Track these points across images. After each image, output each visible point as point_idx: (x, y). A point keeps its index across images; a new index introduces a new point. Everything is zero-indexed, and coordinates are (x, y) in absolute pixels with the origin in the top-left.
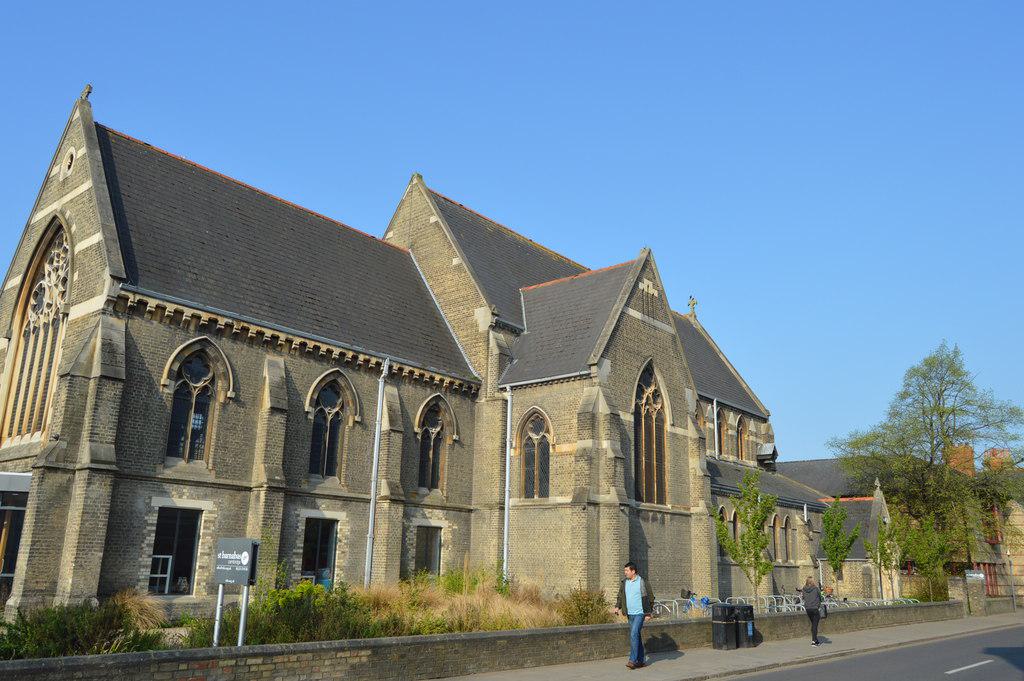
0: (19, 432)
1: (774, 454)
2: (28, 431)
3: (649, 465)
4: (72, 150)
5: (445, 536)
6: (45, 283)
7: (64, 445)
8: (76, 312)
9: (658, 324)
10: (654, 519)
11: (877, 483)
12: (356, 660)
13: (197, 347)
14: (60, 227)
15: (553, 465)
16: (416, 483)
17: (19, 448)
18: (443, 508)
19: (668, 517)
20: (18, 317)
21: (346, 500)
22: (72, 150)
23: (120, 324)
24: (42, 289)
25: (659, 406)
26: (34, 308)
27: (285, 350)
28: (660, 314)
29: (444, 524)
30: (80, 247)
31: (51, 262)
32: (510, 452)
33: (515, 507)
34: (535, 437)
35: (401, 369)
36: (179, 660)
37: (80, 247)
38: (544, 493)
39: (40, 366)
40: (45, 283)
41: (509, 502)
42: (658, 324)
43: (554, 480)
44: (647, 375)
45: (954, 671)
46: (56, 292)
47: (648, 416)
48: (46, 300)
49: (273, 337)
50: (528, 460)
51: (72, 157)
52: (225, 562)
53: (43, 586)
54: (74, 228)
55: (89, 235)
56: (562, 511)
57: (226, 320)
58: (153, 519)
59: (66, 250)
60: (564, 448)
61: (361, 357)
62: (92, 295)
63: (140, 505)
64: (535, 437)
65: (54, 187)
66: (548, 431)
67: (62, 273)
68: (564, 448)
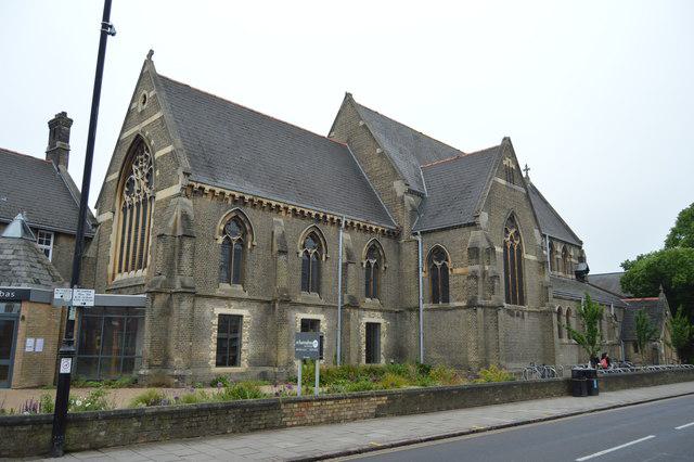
0: (126, 270)
1: (588, 270)
2: (133, 269)
3: (514, 279)
4: (145, 92)
5: (383, 328)
6: (134, 177)
7: (164, 277)
8: (161, 195)
9: (516, 187)
10: (518, 315)
11: (661, 288)
12: (380, 402)
13: (234, 214)
14: (142, 141)
15: (452, 282)
16: (364, 294)
17: (129, 280)
18: (380, 311)
19: (526, 314)
20: (118, 198)
21: (323, 307)
22: (145, 92)
23: (190, 202)
24: (132, 181)
25: (518, 242)
26: (128, 193)
27: (283, 214)
28: (517, 180)
29: (382, 321)
30: (158, 154)
31: (137, 164)
32: (421, 274)
33: (426, 310)
34: (437, 264)
35: (352, 223)
36: (295, 402)
37: (158, 154)
38: (446, 300)
39: (137, 228)
40: (134, 177)
41: (422, 306)
42: (516, 187)
43: (453, 292)
44: (512, 219)
45: (596, 455)
46: (143, 183)
47: (512, 248)
48: (136, 188)
49: (200, 188)
50: (434, 279)
51: (145, 96)
52: (302, 346)
53: (159, 363)
54: (153, 142)
55: (165, 146)
56: (459, 312)
57: (220, 190)
58: (216, 321)
59: (146, 156)
60: (459, 270)
61: (328, 217)
62: (171, 185)
63: (208, 312)
64: (437, 264)
65: (134, 116)
66: (447, 260)
67: (146, 171)
68: (459, 270)
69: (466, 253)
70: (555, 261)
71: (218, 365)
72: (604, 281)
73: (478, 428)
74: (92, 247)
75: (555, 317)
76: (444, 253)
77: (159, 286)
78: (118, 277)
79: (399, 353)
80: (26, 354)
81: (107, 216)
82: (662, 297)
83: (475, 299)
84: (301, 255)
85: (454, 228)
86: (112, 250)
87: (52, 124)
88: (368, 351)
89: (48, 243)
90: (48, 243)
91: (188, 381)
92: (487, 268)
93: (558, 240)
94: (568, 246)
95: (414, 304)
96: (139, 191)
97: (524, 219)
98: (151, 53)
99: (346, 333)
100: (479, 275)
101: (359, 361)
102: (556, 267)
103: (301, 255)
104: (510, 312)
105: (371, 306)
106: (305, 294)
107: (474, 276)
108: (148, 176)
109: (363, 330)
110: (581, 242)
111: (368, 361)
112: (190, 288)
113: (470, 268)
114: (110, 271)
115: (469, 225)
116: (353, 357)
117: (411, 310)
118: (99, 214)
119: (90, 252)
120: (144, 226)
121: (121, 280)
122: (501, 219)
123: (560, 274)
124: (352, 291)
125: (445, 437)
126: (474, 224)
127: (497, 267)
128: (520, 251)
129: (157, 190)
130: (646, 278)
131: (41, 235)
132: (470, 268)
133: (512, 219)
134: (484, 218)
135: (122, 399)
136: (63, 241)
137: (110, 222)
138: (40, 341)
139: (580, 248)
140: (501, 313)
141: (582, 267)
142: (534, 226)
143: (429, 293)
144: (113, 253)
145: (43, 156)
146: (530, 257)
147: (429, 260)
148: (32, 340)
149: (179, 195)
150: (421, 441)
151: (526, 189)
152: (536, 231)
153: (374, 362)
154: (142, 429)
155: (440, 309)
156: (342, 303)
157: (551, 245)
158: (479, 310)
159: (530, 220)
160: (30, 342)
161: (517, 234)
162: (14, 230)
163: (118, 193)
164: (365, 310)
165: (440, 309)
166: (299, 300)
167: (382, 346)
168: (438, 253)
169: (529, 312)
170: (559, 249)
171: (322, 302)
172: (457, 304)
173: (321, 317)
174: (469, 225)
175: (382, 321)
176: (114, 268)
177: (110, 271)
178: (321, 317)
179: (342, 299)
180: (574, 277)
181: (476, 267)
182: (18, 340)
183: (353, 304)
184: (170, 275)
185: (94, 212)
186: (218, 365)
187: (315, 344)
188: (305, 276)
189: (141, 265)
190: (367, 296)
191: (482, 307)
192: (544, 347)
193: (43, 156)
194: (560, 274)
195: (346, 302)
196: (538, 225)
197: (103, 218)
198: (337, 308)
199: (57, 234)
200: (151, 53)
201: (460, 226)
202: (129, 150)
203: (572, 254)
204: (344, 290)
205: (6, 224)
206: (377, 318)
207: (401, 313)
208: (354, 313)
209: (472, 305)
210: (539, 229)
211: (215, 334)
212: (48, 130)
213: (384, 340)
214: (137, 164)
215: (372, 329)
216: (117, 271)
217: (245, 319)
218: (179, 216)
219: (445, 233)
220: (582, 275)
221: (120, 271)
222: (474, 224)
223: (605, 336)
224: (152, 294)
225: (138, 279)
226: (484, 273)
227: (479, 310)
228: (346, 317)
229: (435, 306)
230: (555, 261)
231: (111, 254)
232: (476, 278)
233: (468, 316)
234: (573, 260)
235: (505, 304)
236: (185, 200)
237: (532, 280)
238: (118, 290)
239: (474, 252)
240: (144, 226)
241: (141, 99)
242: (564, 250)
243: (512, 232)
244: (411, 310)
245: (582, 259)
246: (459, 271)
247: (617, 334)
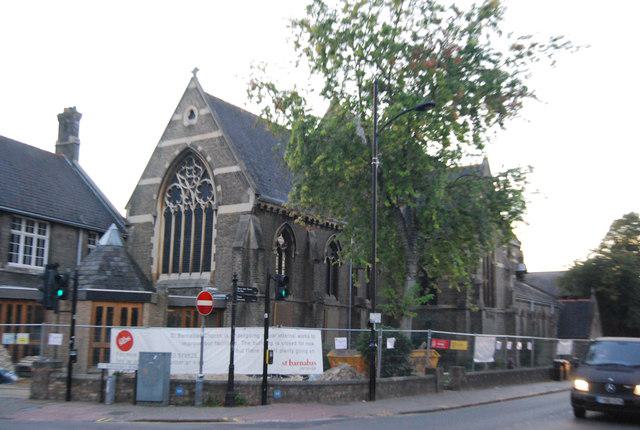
54: (209, 159)
62: (239, 201)
71: (381, 377)
72: (543, 282)
82: (593, 299)
87: (61, 118)
98: (195, 71)
110: (520, 243)
114: (154, 271)
118: (132, 213)
129: (219, 204)
130: (586, 278)
144: (157, 254)
145: (53, 150)
149: (248, 213)
156: (353, 304)
172: (445, 306)
176: (158, 268)
193: (53, 150)
199: (53, 224)
200: (195, 71)
202: (175, 160)
216: (161, 271)
221: (165, 271)
241: (187, 114)
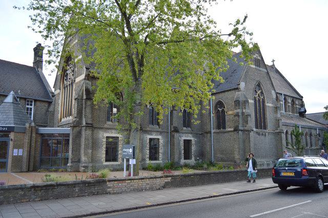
1: (305, 111)
5: (193, 142)
6: (68, 72)
10: (262, 135)
15: (227, 118)
16: (182, 125)
18: (191, 133)
20: (62, 83)
24: (67, 74)
28: (261, 65)
29: (192, 139)
30: (76, 60)
32: (212, 115)
38: (224, 128)
40: (68, 72)
42: (261, 69)
43: (227, 124)
47: (259, 100)
48: (69, 77)
56: (230, 133)
63: (100, 136)
66: (224, 107)
67: (72, 69)
68: (230, 112)
69: (233, 104)
70: (287, 107)
72: (315, 117)
73: (215, 194)
74: (52, 107)
75: (284, 136)
76: (223, 104)
77: (75, 124)
78: (63, 120)
79: (201, 154)
80: (13, 157)
81: (58, 91)
83: (238, 126)
84: (148, 107)
85: (227, 91)
86: (60, 107)
87: (35, 49)
88: (185, 153)
89: (31, 105)
90: (31, 105)
91: (90, 168)
92: (244, 111)
93: (289, 96)
94: (295, 102)
95: (209, 130)
96: (70, 79)
97: (266, 86)
99: (172, 144)
100: (240, 114)
101: (180, 159)
102: (288, 110)
103: (182, 111)
104: (258, 133)
105: (187, 131)
106: (151, 126)
107: (237, 115)
108: (73, 71)
109: (182, 143)
110: (302, 97)
111: (151, 158)
112: (90, 124)
113: (235, 111)
115: (235, 89)
116: (176, 156)
117: (207, 133)
119: (51, 109)
120: (72, 95)
121: (63, 124)
122: (252, 85)
123: (290, 113)
124: (175, 124)
125: (193, 200)
126: (237, 89)
127: (250, 110)
128: (264, 102)
131: (28, 101)
132: (235, 111)
133: (259, 85)
134: (242, 85)
135: (68, 177)
136: (38, 104)
137: (59, 94)
138: (21, 150)
139: (302, 100)
140: (252, 133)
141: (302, 110)
142: (272, 89)
143: (215, 124)
146: (269, 105)
147: (216, 107)
148: (17, 150)
150: (177, 202)
151: (267, 69)
152: (273, 92)
153: (189, 159)
154: (24, 195)
155: (221, 132)
157: (285, 99)
158: (240, 132)
159: (269, 86)
160: (15, 151)
161: (262, 93)
162: (9, 99)
163: (62, 80)
164: (183, 133)
165: (221, 132)
166: (148, 129)
167: (193, 151)
168: (220, 104)
169: (269, 133)
170: (290, 100)
171: (160, 130)
173: (159, 137)
174: (235, 89)
175: (192, 139)
177: (59, 118)
178: (159, 137)
179: (171, 127)
180: (298, 115)
181: (239, 111)
182: (10, 150)
183: (176, 130)
184: (81, 118)
185: (53, 90)
186: (107, 161)
187: (131, 150)
188: (184, 121)
189: (71, 114)
190: (184, 126)
191: (242, 130)
192: (277, 151)
193: (32, 65)
194: (290, 113)
195: (173, 130)
196: (274, 87)
197: (56, 93)
198: (168, 133)
199: (36, 101)
201: (230, 90)
203: (297, 103)
204: (171, 124)
205: (6, 96)
206: (189, 137)
207: (202, 133)
208: (176, 135)
209: (236, 130)
210: (275, 90)
211: (105, 146)
212: (33, 52)
213: (193, 148)
214: (69, 66)
215: (187, 143)
217: (120, 139)
218: (84, 89)
219: (223, 94)
220: (302, 114)
222: (237, 89)
223: (314, 144)
224: (74, 127)
225: (69, 120)
226: (243, 113)
227: (240, 132)
228: (172, 137)
229: (218, 131)
230: (287, 107)
231: (60, 110)
232: (238, 116)
233: (234, 135)
234: (297, 106)
235: (255, 129)
236: (88, 82)
237: (270, 116)
238: (62, 126)
239: (237, 103)
240: (72, 95)
242: (293, 101)
243: (259, 92)
244: (207, 133)
245: (302, 105)
246: (230, 113)
247: (320, 144)
